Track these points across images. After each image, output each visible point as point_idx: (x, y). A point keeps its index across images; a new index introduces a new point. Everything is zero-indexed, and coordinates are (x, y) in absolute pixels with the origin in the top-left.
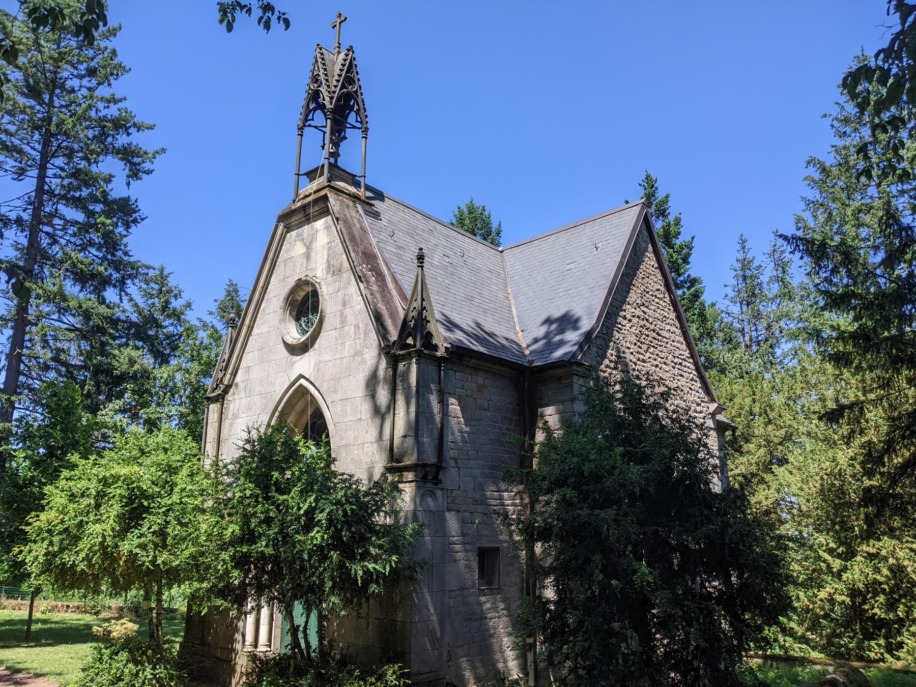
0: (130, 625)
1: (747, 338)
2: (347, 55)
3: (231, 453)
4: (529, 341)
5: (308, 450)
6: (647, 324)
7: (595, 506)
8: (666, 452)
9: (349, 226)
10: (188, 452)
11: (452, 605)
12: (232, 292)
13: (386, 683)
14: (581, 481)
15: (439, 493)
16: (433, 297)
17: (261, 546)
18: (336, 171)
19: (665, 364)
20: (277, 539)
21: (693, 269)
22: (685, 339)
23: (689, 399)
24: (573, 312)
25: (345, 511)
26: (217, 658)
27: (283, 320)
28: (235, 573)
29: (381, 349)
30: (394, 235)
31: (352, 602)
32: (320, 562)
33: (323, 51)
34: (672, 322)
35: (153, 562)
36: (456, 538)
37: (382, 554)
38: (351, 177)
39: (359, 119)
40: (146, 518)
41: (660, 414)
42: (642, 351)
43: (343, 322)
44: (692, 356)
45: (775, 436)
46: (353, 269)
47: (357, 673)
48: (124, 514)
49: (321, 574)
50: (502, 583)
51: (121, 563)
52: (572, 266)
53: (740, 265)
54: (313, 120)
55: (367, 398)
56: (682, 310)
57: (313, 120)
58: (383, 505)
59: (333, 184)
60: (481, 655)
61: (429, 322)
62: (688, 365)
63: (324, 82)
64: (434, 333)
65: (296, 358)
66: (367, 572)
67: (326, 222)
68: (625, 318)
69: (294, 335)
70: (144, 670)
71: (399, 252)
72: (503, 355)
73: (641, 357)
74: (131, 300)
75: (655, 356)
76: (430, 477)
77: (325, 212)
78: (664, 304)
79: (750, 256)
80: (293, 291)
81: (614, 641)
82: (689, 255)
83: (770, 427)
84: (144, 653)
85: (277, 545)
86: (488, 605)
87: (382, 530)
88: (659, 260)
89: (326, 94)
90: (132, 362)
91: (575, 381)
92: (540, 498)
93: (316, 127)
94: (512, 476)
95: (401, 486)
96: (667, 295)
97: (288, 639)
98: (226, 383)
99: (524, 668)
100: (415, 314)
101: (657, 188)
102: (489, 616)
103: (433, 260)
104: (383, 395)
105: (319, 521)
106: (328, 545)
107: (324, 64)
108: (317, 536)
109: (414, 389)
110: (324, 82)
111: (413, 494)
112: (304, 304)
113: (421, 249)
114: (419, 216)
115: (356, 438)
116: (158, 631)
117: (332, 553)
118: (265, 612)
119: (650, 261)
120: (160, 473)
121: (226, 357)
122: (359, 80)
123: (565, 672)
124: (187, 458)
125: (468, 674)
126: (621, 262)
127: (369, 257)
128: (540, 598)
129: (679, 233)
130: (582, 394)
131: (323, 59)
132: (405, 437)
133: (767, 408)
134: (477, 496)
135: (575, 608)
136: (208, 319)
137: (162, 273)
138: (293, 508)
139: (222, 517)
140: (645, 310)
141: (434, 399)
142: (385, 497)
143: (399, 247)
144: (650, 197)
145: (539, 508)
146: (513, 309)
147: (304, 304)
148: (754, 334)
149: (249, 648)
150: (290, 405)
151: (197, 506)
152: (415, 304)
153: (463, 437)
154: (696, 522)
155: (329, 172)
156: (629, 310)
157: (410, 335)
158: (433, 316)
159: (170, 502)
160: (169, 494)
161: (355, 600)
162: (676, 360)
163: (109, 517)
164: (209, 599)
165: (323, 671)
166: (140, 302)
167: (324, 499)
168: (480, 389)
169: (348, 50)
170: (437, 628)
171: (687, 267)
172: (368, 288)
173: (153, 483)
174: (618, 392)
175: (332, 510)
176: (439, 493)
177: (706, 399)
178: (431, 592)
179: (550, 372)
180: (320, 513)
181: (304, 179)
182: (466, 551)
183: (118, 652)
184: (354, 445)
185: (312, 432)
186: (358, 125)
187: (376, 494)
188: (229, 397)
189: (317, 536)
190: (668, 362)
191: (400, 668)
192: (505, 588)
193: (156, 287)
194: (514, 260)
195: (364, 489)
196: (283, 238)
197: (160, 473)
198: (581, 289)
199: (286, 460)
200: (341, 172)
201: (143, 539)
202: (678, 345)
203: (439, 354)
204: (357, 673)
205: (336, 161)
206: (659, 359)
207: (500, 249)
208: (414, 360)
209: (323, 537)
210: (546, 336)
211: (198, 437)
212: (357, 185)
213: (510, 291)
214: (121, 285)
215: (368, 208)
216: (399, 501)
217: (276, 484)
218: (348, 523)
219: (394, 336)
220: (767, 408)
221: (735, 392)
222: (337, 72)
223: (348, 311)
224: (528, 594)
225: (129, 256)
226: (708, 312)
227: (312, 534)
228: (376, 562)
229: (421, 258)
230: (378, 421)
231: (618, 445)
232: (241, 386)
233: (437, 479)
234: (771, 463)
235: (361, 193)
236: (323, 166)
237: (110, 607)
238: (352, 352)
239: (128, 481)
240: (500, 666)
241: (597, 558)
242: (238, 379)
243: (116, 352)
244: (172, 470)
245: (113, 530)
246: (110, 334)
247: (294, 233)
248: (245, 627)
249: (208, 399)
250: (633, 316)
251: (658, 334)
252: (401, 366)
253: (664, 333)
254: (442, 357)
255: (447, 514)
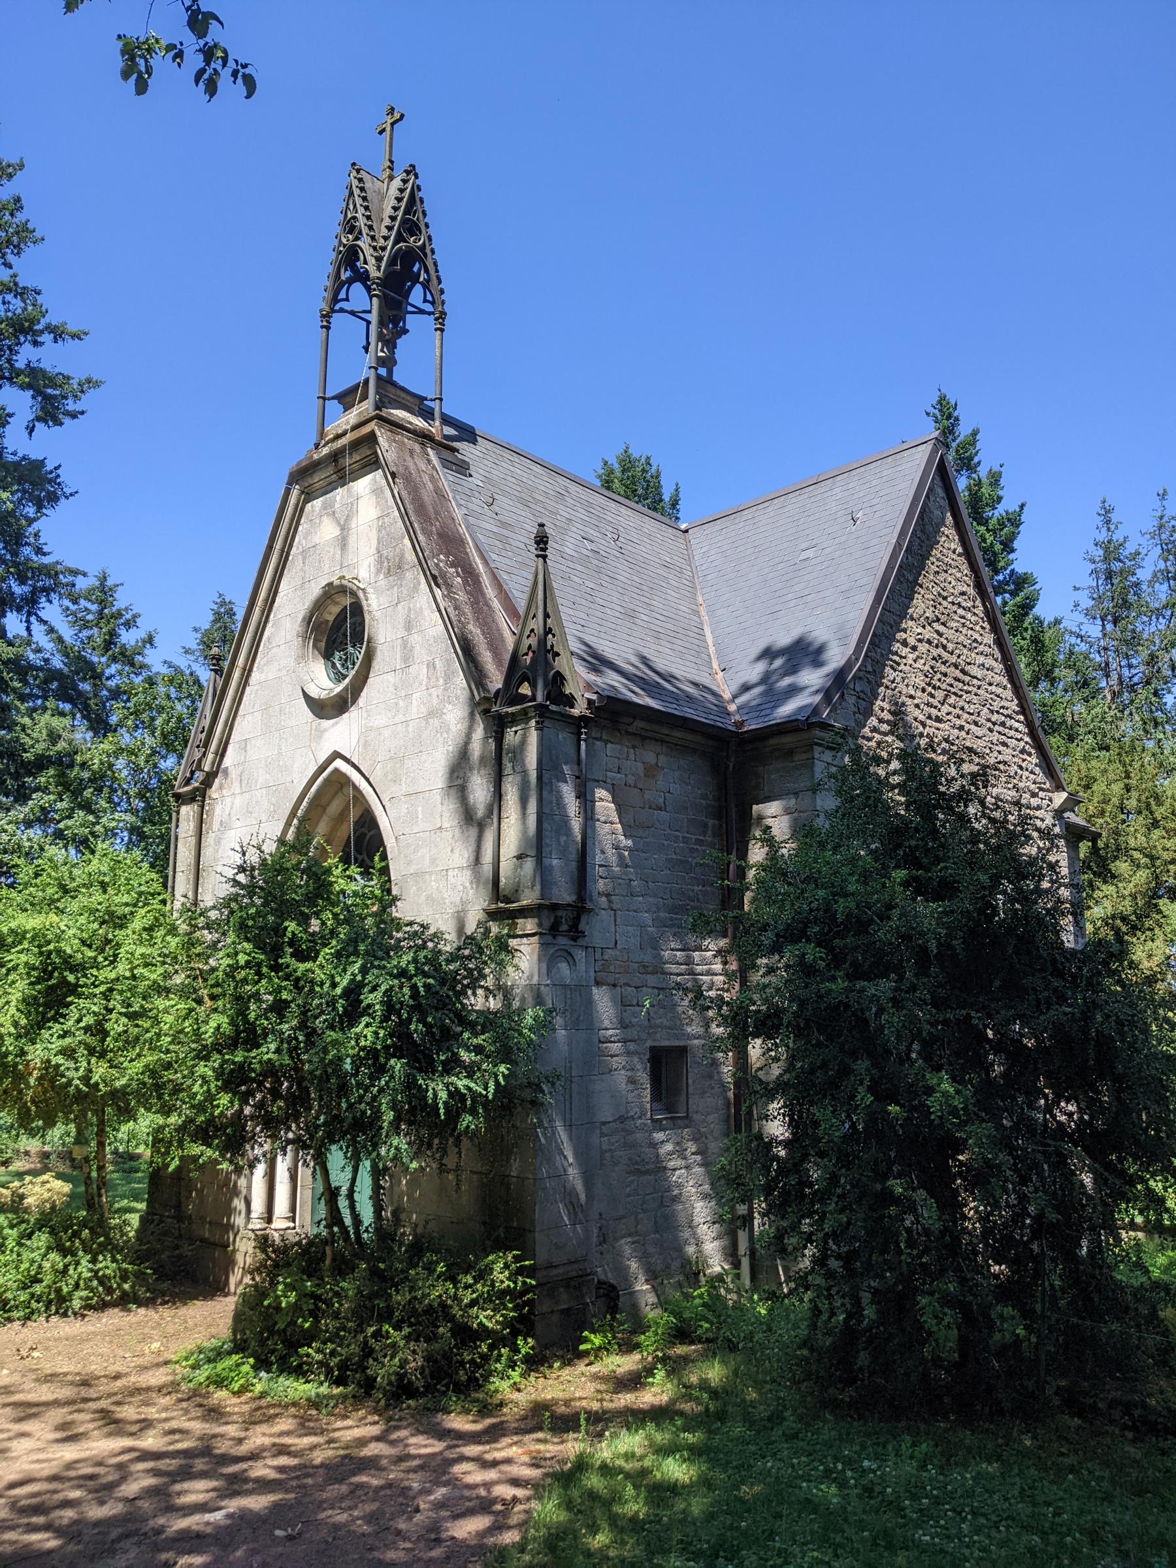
0: (58, 1184)
1: (1114, 680)
2: (405, 181)
3: (214, 890)
4: (734, 687)
5: (348, 883)
6: (945, 655)
7: (857, 973)
8: (984, 878)
9: (413, 487)
10: (143, 888)
11: (605, 1147)
12: (224, 613)
13: (493, 1285)
14: (831, 930)
15: (580, 955)
16: (565, 611)
17: (268, 1051)
18: (389, 390)
19: (976, 724)
20: (296, 1038)
21: (1022, 561)
22: (1012, 680)
23: (1021, 788)
24: (813, 635)
25: (414, 987)
26: (203, 1240)
27: (303, 657)
28: (224, 1099)
29: (474, 705)
30: (494, 501)
31: (430, 1146)
32: (372, 1078)
33: (363, 174)
34: (987, 649)
35: (86, 1079)
36: (611, 1032)
37: (482, 1061)
38: (417, 401)
39: (429, 298)
40: (71, 1003)
41: (971, 810)
42: (935, 702)
43: (408, 659)
44: (1024, 709)
45: (1165, 849)
46: (422, 563)
47: (441, 1268)
48: (35, 998)
49: (374, 1098)
50: (693, 1108)
51: (32, 1081)
52: (810, 553)
53: (1101, 552)
54: (347, 299)
55: (453, 791)
56: (1005, 629)
57: (347, 299)
58: (484, 977)
59: (384, 412)
60: (657, 1232)
61: (558, 654)
62: (1017, 725)
63: (365, 230)
64: (567, 674)
65: (326, 723)
66: (455, 1094)
67: (375, 480)
68: (905, 643)
69: (321, 680)
70: (77, 1263)
71: (505, 532)
72: (689, 712)
73: (934, 712)
74: (51, 630)
75: (957, 711)
76: (564, 927)
77: (372, 463)
78: (973, 619)
79: (1118, 536)
80: (320, 605)
81: (893, 1210)
82: (1012, 537)
83: (1157, 833)
84: (76, 1234)
85: (296, 1048)
86: (669, 1147)
87: (481, 1020)
88: (964, 541)
89: (368, 251)
90: (54, 737)
91: (817, 756)
92: (759, 961)
93: (353, 313)
94: (708, 923)
95: (513, 943)
96: (978, 603)
97: (322, 1212)
98: (207, 769)
99: (731, 1254)
100: (533, 641)
101: (957, 419)
102: (671, 1164)
103: (563, 546)
104: (480, 790)
105: (369, 1006)
106: (386, 1048)
107: (364, 199)
108: (366, 1032)
109: (533, 775)
110: (365, 230)
111: (536, 957)
112: (340, 629)
113: (542, 525)
114: (538, 469)
115: (433, 861)
116: (100, 1196)
117: (392, 1062)
118: (282, 1166)
119: (948, 543)
120: (96, 926)
121: (206, 723)
122: (427, 226)
123: (805, 1263)
124: (143, 898)
125: (634, 1265)
126: (899, 545)
127: (450, 542)
128: (759, 1137)
129: (1000, 499)
130: (831, 776)
131: (362, 189)
132: (519, 857)
133: (1152, 801)
134: (647, 958)
135: (822, 1154)
136: (183, 662)
137: (102, 585)
138: (322, 984)
139: (199, 1002)
140: (941, 628)
141: (568, 793)
142: (485, 963)
143: (504, 525)
144: (948, 432)
145: (756, 977)
146: (708, 631)
147: (340, 629)
148: (1126, 672)
149: (256, 1224)
150: (319, 804)
151: (155, 982)
152: (532, 624)
153: (621, 857)
154: (1038, 1001)
155: (377, 392)
156: (912, 630)
157: (524, 678)
158: (566, 645)
159: (113, 975)
160: (112, 962)
161: (436, 1141)
162: (995, 717)
163: (8, 1003)
164: (181, 1145)
165: (382, 1266)
166: (67, 633)
167: (379, 967)
168: (651, 771)
169: (408, 172)
170: (580, 1187)
171: (1011, 556)
172: (448, 596)
173: (83, 942)
174: (895, 773)
175: (392, 987)
176: (580, 955)
177: (1048, 786)
178: (569, 1127)
179: (773, 741)
180: (371, 992)
181: (334, 406)
182: (628, 1053)
183: (32, 1233)
184: (430, 873)
185: (358, 850)
186: (428, 307)
187: (469, 958)
188: (213, 792)
189: (366, 1032)
190: (982, 720)
191: (517, 1259)
192: (697, 1117)
193: (94, 607)
194: (707, 546)
195: (448, 948)
196: (299, 512)
197: (96, 926)
198: (827, 593)
199: (311, 900)
200: (399, 392)
201: (68, 1040)
202: (999, 691)
203: (576, 712)
204: (441, 1268)
205: (390, 372)
206: (966, 716)
207: (683, 527)
208: (533, 723)
209: (376, 1033)
210: (765, 679)
211: (162, 862)
212: (428, 415)
213: (700, 600)
214: (28, 606)
215: (446, 454)
216: (510, 969)
217: (291, 943)
218: (418, 1008)
219: (496, 681)
220: (1152, 801)
221: (1093, 773)
222: (389, 211)
223: (415, 638)
224: (738, 1130)
225: (45, 554)
226: (1048, 636)
227: (358, 1030)
228: (470, 1076)
229: (542, 541)
230: (473, 832)
231: (897, 867)
232: (234, 773)
233: (577, 931)
234: (1156, 896)
235: (435, 428)
236: (367, 381)
237: (27, 1153)
238: (424, 710)
239: (39, 938)
240: (691, 1250)
241: (862, 1065)
242: (227, 762)
243: (26, 720)
244: (116, 920)
245: (16, 1024)
246: (14, 690)
247: (318, 503)
248: (249, 1187)
249: (178, 797)
250: (920, 641)
251: (963, 672)
252: (511, 736)
253: (974, 670)
254: (582, 718)
255: (595, 990)
